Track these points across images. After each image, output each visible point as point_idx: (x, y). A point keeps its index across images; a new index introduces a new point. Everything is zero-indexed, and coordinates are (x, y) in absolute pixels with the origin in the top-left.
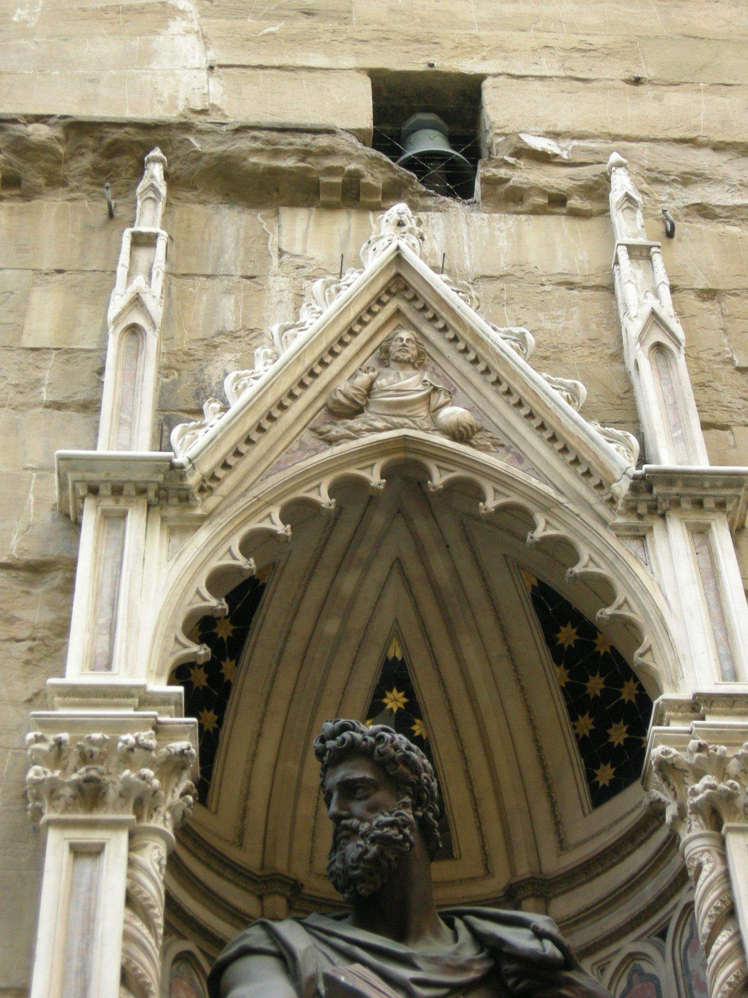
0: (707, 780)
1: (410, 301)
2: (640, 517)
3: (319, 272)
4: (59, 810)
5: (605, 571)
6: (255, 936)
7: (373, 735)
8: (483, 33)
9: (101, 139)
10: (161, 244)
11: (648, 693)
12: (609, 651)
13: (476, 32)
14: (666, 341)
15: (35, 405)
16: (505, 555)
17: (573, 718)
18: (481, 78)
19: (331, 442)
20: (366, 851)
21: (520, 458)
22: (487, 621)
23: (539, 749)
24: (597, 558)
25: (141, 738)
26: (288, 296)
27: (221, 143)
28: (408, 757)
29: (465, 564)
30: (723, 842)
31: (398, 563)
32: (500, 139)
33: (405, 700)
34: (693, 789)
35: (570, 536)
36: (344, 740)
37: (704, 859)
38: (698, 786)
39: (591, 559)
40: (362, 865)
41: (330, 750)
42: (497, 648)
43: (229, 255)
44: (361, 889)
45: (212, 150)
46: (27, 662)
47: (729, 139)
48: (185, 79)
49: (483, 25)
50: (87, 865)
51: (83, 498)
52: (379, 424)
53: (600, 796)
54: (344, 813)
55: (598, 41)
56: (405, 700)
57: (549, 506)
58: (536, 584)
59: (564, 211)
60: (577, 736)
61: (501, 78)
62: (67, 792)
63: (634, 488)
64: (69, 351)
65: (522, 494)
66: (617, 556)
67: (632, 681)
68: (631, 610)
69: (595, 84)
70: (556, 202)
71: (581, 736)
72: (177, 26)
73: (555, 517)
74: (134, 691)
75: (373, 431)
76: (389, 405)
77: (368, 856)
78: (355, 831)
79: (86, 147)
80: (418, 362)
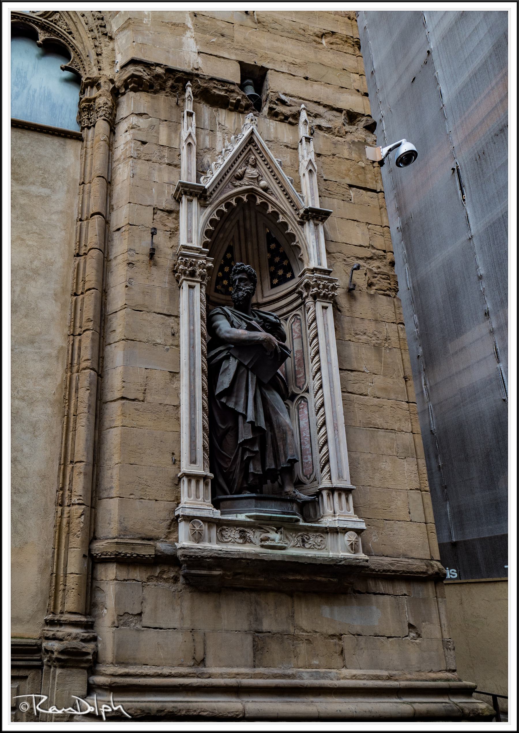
0: (316, 289)
1: (254, 146)
2: (303, 219)
3: (231, 132)
5: (294, 233)
6: (219, 310)
8: (268, 52)
9: (175, 76)
10: (194, 116)
13: (266, 51)
14: (313, 169)
15: (164, 164)
18: (267, 69)
19: (236, 187)
21: (277, 198)
22: (255, 240)
26: (221, 139)
27: (205, 83)
29: (253, 224)
30: (315, 303)
31: (238, 222)
32: (272, 94)
35: (288, 222)
38: (313, 290)
42: (255, 247)
43: (207, 123)
45: (203, 85)
47: (328, 104)
48: (192, 55)
49: (269, 49)
50: (191, 289)
51: (182, 195)
52: (247, 183)
53: (273, 286)
55: (298, 61)
57: (284, 213)
59: (287, 122)
61: (273, 71)
62: (187, 272)
63: (304, 212)
64: (170, 148)
65: (278, 209)
66: (298, 229)
69: (296, 77)
70: (286, 118)
72: (188, 34)
73: (284, 216)
75: (245, 185)
76: (250, 178)
78: (241, 290)
79: (170, 77)
80: (255, 166)
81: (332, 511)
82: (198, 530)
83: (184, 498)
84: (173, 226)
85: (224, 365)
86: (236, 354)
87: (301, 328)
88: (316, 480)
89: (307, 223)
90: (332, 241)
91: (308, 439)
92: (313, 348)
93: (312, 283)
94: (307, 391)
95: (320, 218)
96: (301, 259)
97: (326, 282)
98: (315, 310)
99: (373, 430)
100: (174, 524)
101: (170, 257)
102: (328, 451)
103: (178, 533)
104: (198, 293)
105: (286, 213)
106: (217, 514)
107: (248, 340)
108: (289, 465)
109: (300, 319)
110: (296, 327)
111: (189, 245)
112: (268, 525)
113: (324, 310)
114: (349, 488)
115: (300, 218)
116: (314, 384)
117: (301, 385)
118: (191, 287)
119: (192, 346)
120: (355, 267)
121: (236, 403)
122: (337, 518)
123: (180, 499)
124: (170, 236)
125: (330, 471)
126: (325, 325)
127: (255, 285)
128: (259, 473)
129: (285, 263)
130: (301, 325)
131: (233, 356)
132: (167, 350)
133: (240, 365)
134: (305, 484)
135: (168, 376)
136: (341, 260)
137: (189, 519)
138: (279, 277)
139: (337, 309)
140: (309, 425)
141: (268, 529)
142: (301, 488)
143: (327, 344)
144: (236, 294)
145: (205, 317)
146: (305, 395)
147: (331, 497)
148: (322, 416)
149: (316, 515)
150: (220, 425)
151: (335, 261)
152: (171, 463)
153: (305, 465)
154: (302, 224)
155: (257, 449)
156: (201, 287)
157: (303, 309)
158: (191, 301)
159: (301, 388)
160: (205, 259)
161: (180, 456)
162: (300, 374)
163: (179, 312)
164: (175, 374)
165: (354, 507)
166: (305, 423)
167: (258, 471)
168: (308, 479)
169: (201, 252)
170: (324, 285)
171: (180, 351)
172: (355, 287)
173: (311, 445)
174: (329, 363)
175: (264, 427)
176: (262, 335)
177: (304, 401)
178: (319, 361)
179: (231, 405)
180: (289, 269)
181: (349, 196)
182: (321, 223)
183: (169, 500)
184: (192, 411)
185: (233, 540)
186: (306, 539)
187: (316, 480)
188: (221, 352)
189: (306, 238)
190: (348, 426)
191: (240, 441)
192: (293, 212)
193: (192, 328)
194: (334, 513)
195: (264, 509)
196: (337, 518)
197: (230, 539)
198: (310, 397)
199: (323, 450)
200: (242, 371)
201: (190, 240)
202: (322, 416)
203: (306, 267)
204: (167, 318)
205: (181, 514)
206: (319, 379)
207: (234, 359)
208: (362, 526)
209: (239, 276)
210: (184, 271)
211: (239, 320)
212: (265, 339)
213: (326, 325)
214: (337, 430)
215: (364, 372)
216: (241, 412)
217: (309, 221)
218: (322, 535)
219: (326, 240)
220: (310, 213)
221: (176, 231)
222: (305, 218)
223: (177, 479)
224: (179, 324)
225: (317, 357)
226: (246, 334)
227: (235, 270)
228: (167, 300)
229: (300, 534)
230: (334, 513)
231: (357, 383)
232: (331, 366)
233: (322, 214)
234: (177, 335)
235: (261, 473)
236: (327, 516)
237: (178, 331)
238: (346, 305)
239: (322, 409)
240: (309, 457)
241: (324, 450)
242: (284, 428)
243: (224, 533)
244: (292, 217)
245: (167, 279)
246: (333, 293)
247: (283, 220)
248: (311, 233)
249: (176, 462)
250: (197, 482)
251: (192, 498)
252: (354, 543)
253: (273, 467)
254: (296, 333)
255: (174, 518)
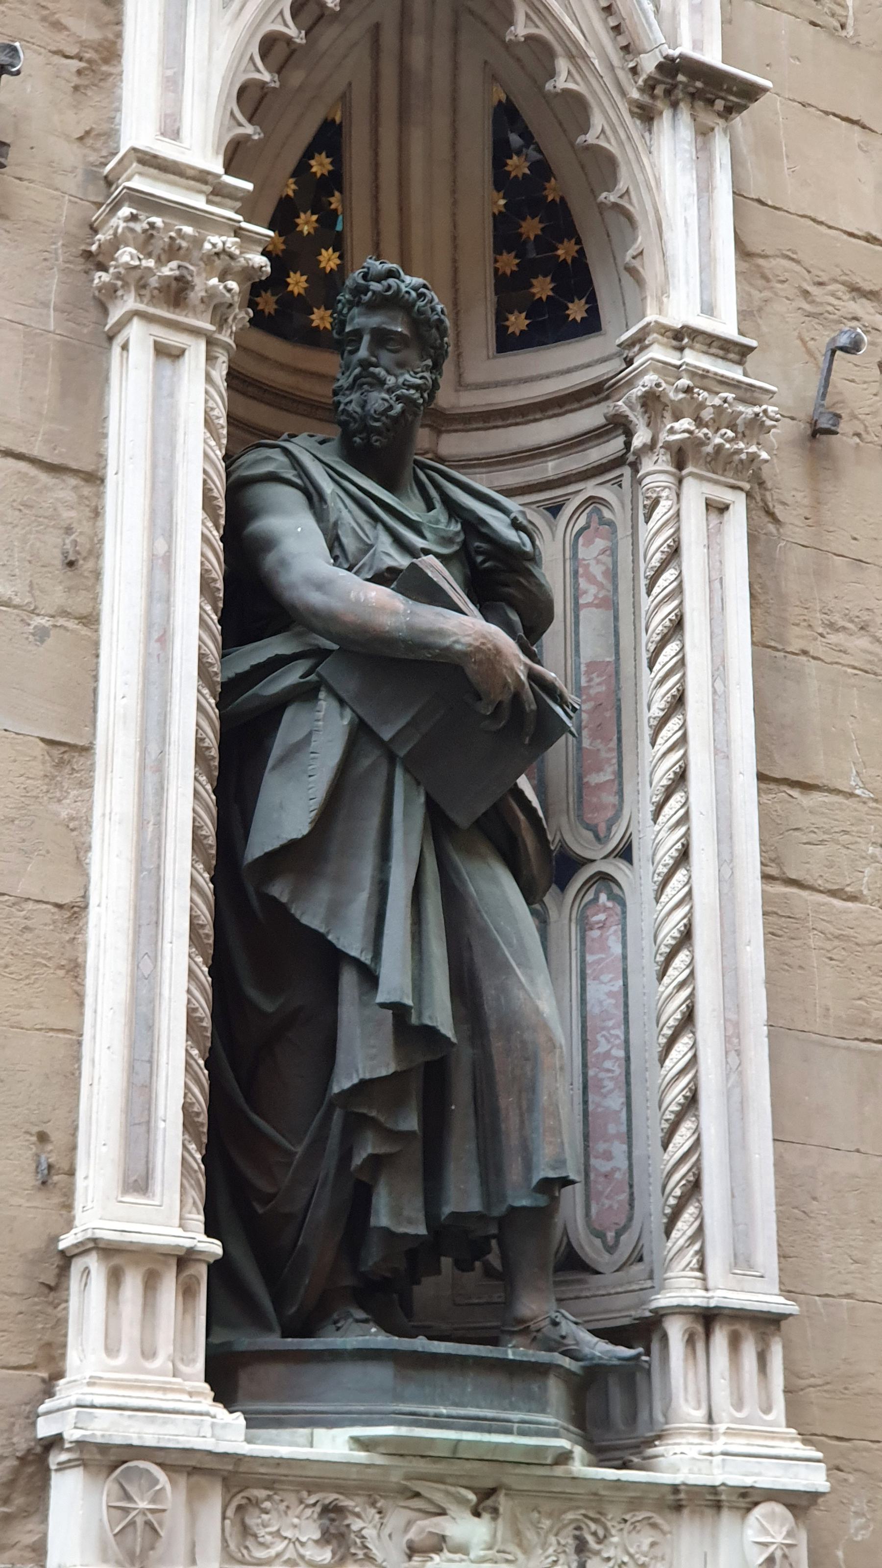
0: (685, 423)
2: (653, 97)
4: (146, 300)
7: (415, 289)
11: (589, 261)
12: (558, 200)
16: (486, 62)
17: (498, 250)
20: (391, 407)
22: (441, 122)
23: (455, 270)
24: (609, 132)
25: (228, 245)
28: (441, 321)
29: (442, 55)
30: (680, 481)
33: (331, 168)
34: (672, 428)
36: (389, 287)
37: (664, 494)
38: (677, 425)
39: (603, 131)
40: (384, 418)
41: (374, 292)
44: (376, 441)
46: (76, 88)
50: (166, 362)
53: (507, 343)
54: (374, 359)
56: (331, 168)
57: (576, 55)
58: (504, 101)
60: (496, 270)
63: (660, 67)
66: (629, 138)
67: (573, 241)
68: (631, 203)
71: (500, 273)
74: (210, 178)
77: (392, 413)
78: (380, 383)
81: (701, 1413)
82: (143, 1512)
83: (86, 1358)
84: (91, 33)
85: (292, 726)
86: (348, 686)
87: (615, 563)
88: (641, 1259)
89: (667, 114)
90: (759, 201)
91: (618, 1071)
92: (661, 682)
93: (672, 395)
94: (625, 853)
95: (719, 104)
96: (632, 271)
97: (730, 396)
98: (678, 514)
99: (871, 1052)
100: (31, 1476)
101: (71, 184)
102: (697, 1143)
103: (45, 1520)
104: (197, 390)
105: (585, 57)
106: (225, 1431)
107: (404, 641)
108: (542, 1201)
109: (611, 524)
110: (591, 551)
111: (167, 150)
112: (440, 1479)
113: (714, 518)
114: (775, 1309)
115: (641, 90)
116: (657, 841)
117: (600, 819)
118: (166, 353)
119: (158, 636)
120: (843, 340)
121: (335, 911)
122: (718, 1446)
123: (63, 1356)
124: (76, 80)
125: (700, 1232)
126: (716, 582)
127: (436, 367)
128: (411, 1230)
129: (565, 251)
130: (613, 551)
131: (332, 692)
132: (42, 634)
133: (360, 734)
134: (598, 1273)
135: (38, 760)
136: (791, 292)
137: (109, 1460)
138: (534, 309)
139: (764, 512)
140: (626, 1005)
141: (439, 1498)
142: (570, 1291)
143: (719, 669)
144: (355, 396)
145: (222, 503)
146: (617, 869)
147: (700, 1346)
148: (682, 985)
149: (632, 1418)
150: (253, 993)
151: (767, 294)
152: (31, 1180)
153: (599, 1184)
154: (646, 116)
155: (411, 1123)
156: (210, 359)
157: (626, 481)
158: (163, 418)
159: (602, 829)
160: (238, 232)
161: (74, 1148)
162: (599, 770)
163: (101, 457)
164: (71, 754)
165: (788, 1391)
166: (610, 994)
167: (410, 1221)
168: (611, 1249)
169: (218, 192)
170: (719, 410)
171: (97, 644)
172: (836, 424)
173: (628, 1097)
174: (722, 753)
175: (447, 1029)
176: (466, 627)
177: (612, 897)
178: (683, 740)
179: (312, 917)
180: (577, 280)
181: (839, 10)
182: (721, 122)
183: (13, 1360)
184: (143, 941)
185: (290, 1554)
186: (590, 1539)
187: (641, 1259)
188: (278, 663)
189: (658, 182)
190: (777, 1032)
191: (342, 1083)
192: (615, 57)
193: (161, 547)
194: (710, 1419)
195: (431, 1410)
196: (718, 1446)
197: (280, 1546)
198: (637, 880)
199: (677, 1139)
200: (365, 763)
201: (171, 130)
202: (682, 985)
203: (651, 317)
204: (44, 478)
205: (71, 1435)
206: (678, 824)
207: (335, 704)
208: (813, 1478)
209: (375, 320)
210: (137, 274)
211: (362, 517)
212: (478, 649)
213: (717, 585)
214: (738, 1053)
215: (852, 795)
216: (354, 953)
217: (675, 105)
218: (658, 1520)
219: (737, 194)
220: (681, 78)
221: (106, 61)
222: (659, 91)
223: (57, 1261)
224: (97, 513)
225: (674, 724)
226: (395, 613)
227: (359, 291)
228: (48, 389)
229: (570, 1516)
230: (710, 1419)
231: (822, 842)
232: (729, 766)
233: (729, 91)
234: (86, 566)
235: (422, 1230)
236: (680, 1432)
237: (95, 551)
238: (799, 496)
239: (682, 957)
240: (619, 1149)
241: (682, 1140)
242: (527, 1036)
243: (253, 1520)
244: (608, 80)
245: (53, 287)
246: (753, 449)
247: (571, 86)
248: (679, 165)
249: (55, 1177)
250: (151, 1282)
251: (121, 1360)
252: (778, 1555)
253: (475, 1205)
254: (592, 579)
255: (29, 1451)
